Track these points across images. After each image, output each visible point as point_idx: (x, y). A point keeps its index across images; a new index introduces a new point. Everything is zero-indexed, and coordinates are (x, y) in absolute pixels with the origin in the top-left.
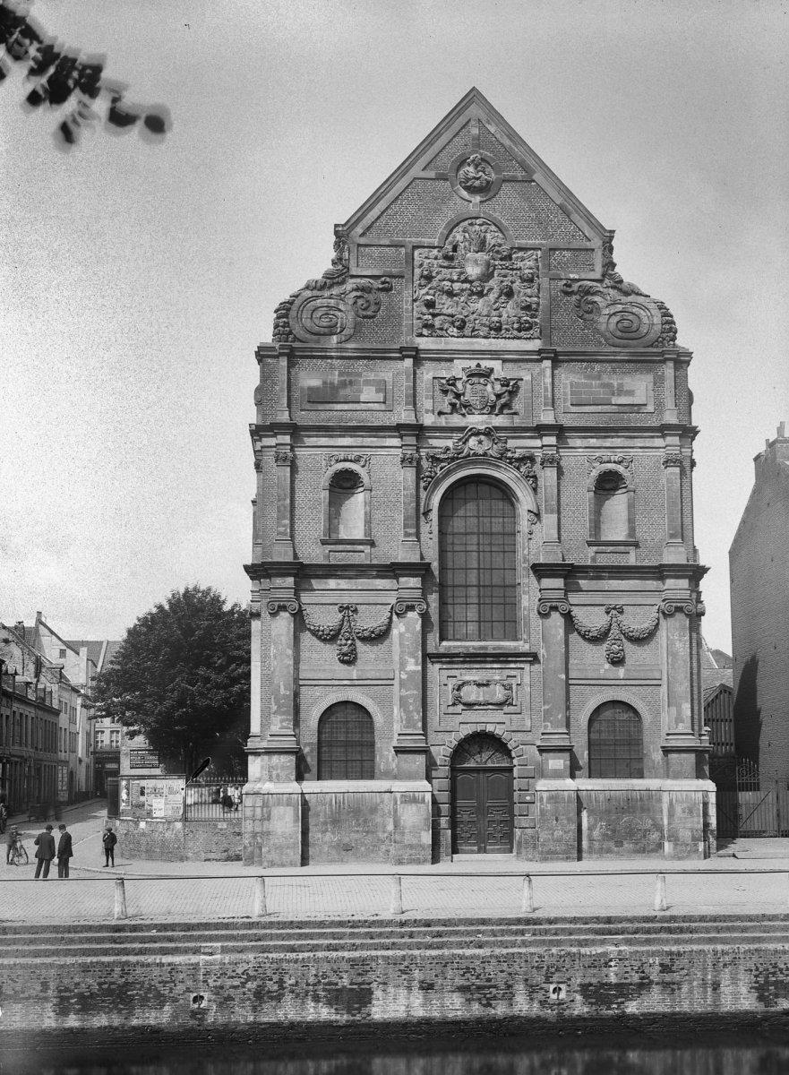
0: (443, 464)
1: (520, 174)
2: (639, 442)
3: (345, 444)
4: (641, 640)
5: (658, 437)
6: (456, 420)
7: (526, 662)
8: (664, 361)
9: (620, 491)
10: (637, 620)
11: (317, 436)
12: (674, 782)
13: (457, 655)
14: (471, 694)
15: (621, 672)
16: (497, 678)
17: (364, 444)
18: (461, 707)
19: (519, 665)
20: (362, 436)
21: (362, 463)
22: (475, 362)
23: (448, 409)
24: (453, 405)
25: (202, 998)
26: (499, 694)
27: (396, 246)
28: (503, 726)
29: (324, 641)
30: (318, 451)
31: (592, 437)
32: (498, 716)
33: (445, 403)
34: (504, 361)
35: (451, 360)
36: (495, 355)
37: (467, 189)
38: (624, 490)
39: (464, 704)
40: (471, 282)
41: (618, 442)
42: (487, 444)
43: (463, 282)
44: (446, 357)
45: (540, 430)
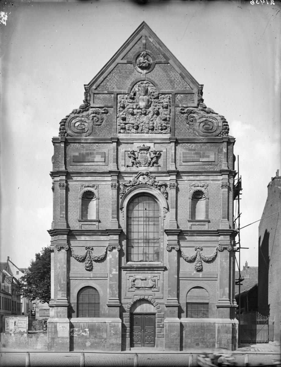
3: (88, 180)
6: (134, 169)
14: (139, 283)
15: (200, 274)
19: (158, 272)
26: (150, 284)
28: (151, 297)
30: (77, 183)
31: (191, 176)
32: (150, 292)
35: (132, 143)
36: (151, 140)
37: (140, 67)
41: (202, 178)
44: (130, 142)
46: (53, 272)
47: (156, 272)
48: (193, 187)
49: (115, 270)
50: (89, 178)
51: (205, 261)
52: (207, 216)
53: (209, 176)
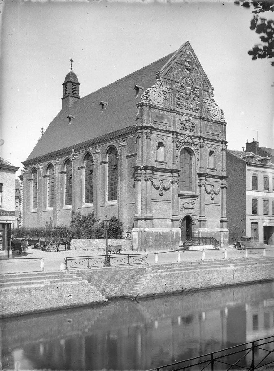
0: (181, 143)
1: (196, 68)
2: (217, 144)
3: (161, 134)
4: (167, 189)
5: (171, 134)
6: (183, 132)
7: (196, 198)
8: (147, 106)
9: (212, 156)
10: (167, 184)
11: (155, 131)
12: (175, 229)
13: (183, 195)
14: (186, 206)
15: (213, 202)
16: (191, 202)
17: (165, 135)
18: (184, 209)
19: (195, 199)
20: (164, 133)
21: (164, 140)
22: (188, 117)
23: (182, 129)
24: (183, 128)
25: (71, 295)
26: (191, 206)
27: (171, 80)
28: (192, 214)
29: (156, 188)
30: (155, 135)
31: (209, 141)
32: (190, 211)
33: (181, 126)
34: (193, 118)
35: (182, 115)
36: (191, 115)
37: (187, 69)
38: (164, 147)
39: (185, 208)
40: (187, 95)
41: (213, 143)
42: (190, 140)
43: (185, 94)
44: (181, 114)
45: (200, 138)
46: (140, 195)
47: (194, 199)
48: (210, 148)
49: (176, 196)
50: (161, 133)
51: (164, 189)
52: (165, 159)
53: (216, 142)
